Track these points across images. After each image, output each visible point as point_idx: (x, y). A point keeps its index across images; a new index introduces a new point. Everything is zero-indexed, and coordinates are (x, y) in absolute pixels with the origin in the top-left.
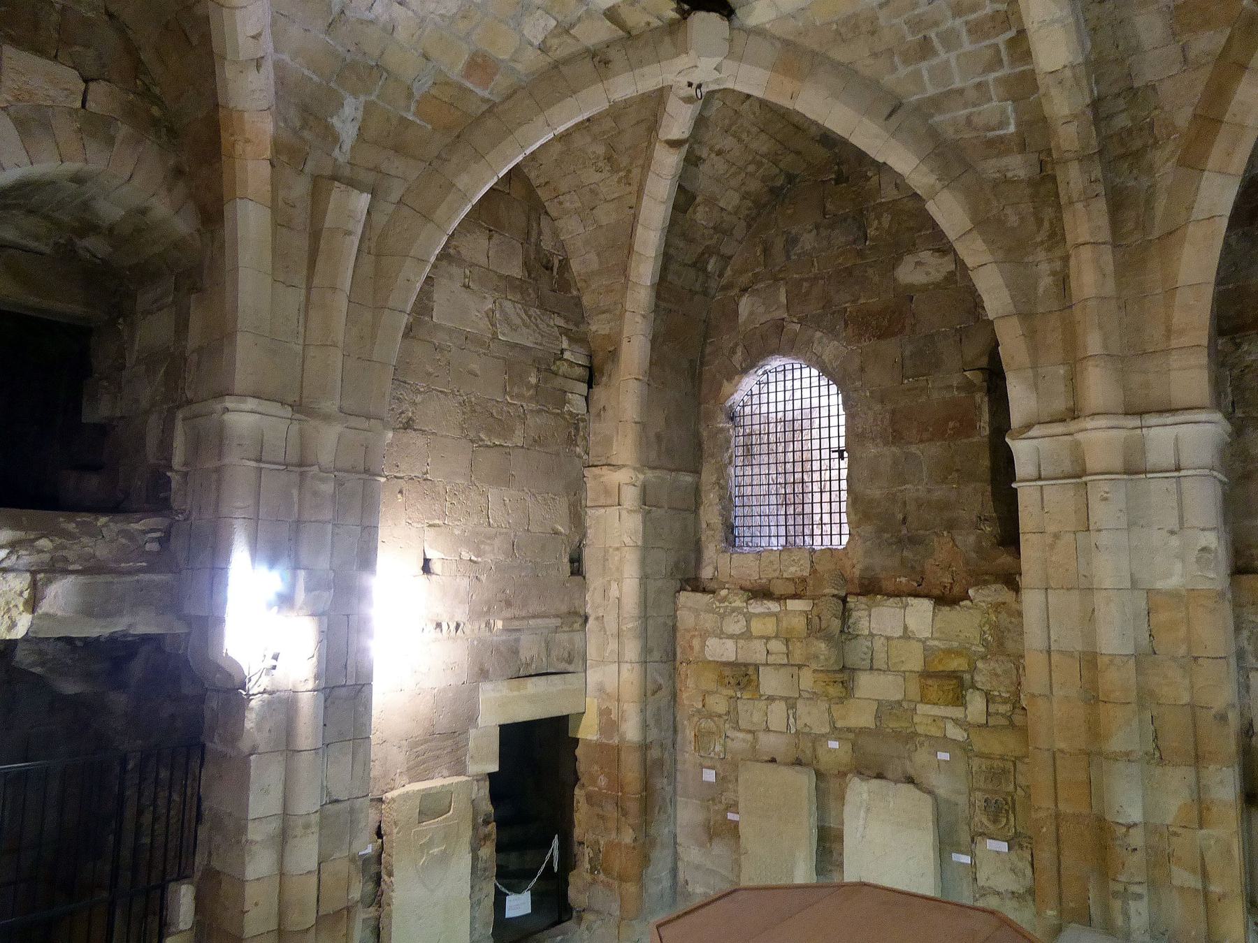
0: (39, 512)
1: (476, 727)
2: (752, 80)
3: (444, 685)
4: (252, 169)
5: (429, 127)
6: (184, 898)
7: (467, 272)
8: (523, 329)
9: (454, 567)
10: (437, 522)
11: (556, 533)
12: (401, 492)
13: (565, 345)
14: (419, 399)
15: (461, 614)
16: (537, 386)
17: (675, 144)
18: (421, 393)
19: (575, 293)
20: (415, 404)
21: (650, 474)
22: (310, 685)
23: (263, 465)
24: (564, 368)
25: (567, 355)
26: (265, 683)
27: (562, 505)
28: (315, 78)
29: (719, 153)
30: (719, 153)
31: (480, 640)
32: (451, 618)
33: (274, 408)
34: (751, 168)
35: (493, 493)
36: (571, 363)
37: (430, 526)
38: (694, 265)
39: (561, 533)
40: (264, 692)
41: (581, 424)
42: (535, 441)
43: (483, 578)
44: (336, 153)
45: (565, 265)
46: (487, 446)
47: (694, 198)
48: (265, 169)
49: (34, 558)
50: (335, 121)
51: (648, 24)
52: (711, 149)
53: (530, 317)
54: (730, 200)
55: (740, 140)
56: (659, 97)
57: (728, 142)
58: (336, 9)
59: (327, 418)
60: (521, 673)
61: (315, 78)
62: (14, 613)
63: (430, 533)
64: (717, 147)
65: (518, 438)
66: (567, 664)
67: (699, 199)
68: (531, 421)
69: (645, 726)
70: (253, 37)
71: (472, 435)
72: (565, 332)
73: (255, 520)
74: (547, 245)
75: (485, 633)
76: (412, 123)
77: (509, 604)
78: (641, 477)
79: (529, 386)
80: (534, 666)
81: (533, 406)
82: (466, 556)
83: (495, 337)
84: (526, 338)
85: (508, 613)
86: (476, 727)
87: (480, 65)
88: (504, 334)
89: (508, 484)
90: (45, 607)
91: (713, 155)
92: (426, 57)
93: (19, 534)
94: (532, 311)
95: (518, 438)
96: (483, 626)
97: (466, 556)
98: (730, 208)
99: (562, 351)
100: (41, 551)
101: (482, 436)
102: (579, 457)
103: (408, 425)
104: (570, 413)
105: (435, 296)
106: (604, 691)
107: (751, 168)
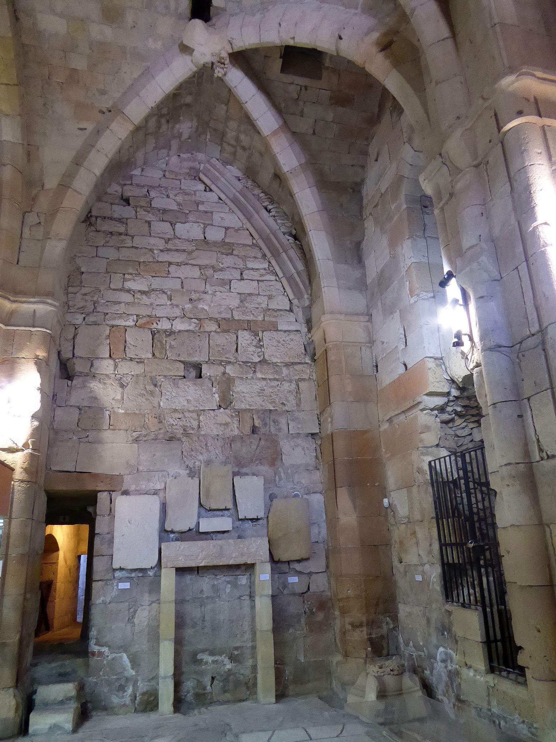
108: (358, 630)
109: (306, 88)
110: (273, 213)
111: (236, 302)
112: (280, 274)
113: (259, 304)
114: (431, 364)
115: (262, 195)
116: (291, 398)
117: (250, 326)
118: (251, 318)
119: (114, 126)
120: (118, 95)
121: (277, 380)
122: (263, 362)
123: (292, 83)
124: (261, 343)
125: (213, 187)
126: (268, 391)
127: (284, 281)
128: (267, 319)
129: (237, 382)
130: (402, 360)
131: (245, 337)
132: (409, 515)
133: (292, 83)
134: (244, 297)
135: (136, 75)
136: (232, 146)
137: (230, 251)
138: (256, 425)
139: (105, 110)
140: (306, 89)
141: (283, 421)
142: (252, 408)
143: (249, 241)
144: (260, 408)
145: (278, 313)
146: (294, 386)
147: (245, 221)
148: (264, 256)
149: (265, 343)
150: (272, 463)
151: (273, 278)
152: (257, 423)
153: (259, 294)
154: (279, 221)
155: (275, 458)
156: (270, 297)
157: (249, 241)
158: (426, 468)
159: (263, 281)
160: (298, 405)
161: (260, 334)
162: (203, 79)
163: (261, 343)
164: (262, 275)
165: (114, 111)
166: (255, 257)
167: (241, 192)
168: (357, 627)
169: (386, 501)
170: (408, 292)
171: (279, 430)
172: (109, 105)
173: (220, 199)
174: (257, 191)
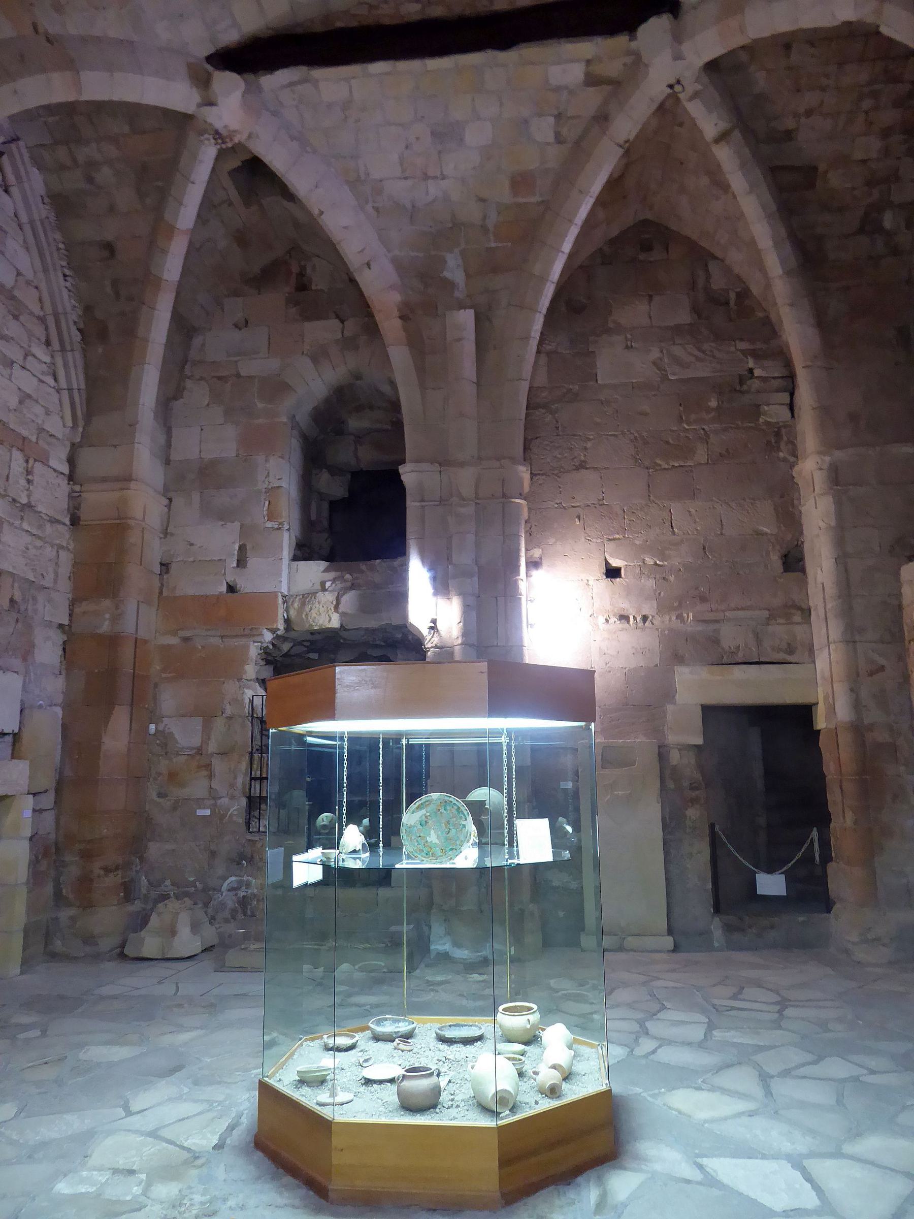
0: (350, 563)
1: (675, 704)
2: (708, 44)
3: (633, 666)
4: (391, 326)
5: (509, 244)
6: (310, 740)
7: (629, 336)
8: (696, 364)
9: (638, 570)
10: (617, 536)
11: (759, 533)
12: (579, 518)
13: (751, 364)
14: (589, 445)
15: (648, 609)
16: (718, 408)
17: (722, 137)
18: (589, 439)
19: (760, 314)
20: (586, 449)
21: (839, 455)
22: (460, 641)
23: (424, 504)
24: (755, 384)
25: (757, 372)
26: (436, 640)
27: (766, 508)
28: (421, 255)
29: (809, 113)
30: (809, 113)
31: (671, 630)
32: (639, 611)
33: (425, 466)
34: (867, 104)
35: (676, 509)
36: (764, 379)
37: (610, 540)
38: (861, 230)
39: (766, 534)
40: (436, 647)
41: (783, 431)
42: (721, 455)
43: (672, 578)
44: (457, 294)
45: (744, 294)
46: (665, 469)
47: (815, 169)
48: (398, 323)
49: (343, 585)
50: (446, 274)
51: (625, 65)
52: (796, 115)
53: (704, 352)
54: (868, 147)
55: (823, 89)
56: (668, 110)
57: (810, 99)
58: (409, 206)
59: (462, 465)
60: (725, 660)
61: (421, 255)
62: (330, 612)
63: (610, 546)
64: (802, 110)
65: (701, 455)
66: (796, 653)
67: (822, 167)
68: (713, 439)
69: (857, 705)
70: (359, 252)
71: (647, 463)
72: (757, 355)
73: (421, 539)
74: (718, 283)
75: (676, 624)
76: (497, 247)
77: (703, 599)
78: (827, 459)
79: (709, 410)
80: (740, 654)
81: (717, 426)
82: (649, 561)
83: (664, 378)
84: (703, 371)
85: (700, 607)
86: (675, 704)
87: (521, 182)
88: (674, 374)
89: (693, 497)
90: (342, 608)
91: (803, 120)
92: (482, 200)
93: (338, 574)
94: (706, 346)
95: (701, 455)
96: (674, 618)
97: (649, 561)
98: (874, 155)
99: (751, 371)
100: (345, 581)
101: (659, 462)
102: (785, 460)
103: (582, 466)
104: (768, 424)
105: (598, 364)
106: (825, 679)
107: (867, 104)
108: (111, 875)
109: (231, 204)
110: (68, 284)
111: (13, 402)
112: (63, 384)
113: (36, 415)
114: (280, 601)
115: (61, 246)
116: (51, 570)
117: (22, 444)
118: (25, 433)
119: (56, 77)
120: (72, 30)
121: (39, 538)
122: (29, 506)
123: (225, 189)
124: (30, 477)
125: (14, 190)
126: (33, 551)
127: (65, 394)
128: (41, 442)
129: (5, 526)
130: (230, 578)
131: (17, 456)
132: (201, 746)
133: (225, 189)
134: (25, 398)
135: (112, 33)
136: (75, 160)
137: (17, 313)
138: (15, 598)
139: (41, 30)
140: (229, 205)
141: (41, 598)
142: (15, 572)
143: (37, 311)
144: (22, 575)
145: (54, 440)
146: (54, 553)
147: (41, 275)
148: (48, 343)
149: (36, 478)
150: (25, 659)
151: (52, 382)
152: (18, 596)
153: (37, 401)
154: (73, 301)
155: (27, 653)
156: (48, 413)
157: (37, 311)
158: (247, 701)
159: (43, 382)
160: (55, 581)
161: (31, 461)
162: (180, 123)
163: (30, 477)
164: (43, 373)
165: (62, 54)
166: (39, 339)
167: (41, 220)
168: (111, 871)
169: (152, 727)
170: (265, 513)
171: (35, 611)
172: (53, 30)
173: (16, 215)
174: (58, 236)
